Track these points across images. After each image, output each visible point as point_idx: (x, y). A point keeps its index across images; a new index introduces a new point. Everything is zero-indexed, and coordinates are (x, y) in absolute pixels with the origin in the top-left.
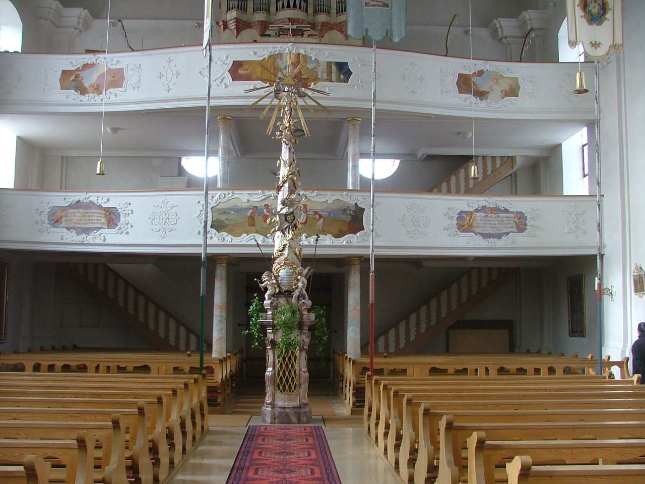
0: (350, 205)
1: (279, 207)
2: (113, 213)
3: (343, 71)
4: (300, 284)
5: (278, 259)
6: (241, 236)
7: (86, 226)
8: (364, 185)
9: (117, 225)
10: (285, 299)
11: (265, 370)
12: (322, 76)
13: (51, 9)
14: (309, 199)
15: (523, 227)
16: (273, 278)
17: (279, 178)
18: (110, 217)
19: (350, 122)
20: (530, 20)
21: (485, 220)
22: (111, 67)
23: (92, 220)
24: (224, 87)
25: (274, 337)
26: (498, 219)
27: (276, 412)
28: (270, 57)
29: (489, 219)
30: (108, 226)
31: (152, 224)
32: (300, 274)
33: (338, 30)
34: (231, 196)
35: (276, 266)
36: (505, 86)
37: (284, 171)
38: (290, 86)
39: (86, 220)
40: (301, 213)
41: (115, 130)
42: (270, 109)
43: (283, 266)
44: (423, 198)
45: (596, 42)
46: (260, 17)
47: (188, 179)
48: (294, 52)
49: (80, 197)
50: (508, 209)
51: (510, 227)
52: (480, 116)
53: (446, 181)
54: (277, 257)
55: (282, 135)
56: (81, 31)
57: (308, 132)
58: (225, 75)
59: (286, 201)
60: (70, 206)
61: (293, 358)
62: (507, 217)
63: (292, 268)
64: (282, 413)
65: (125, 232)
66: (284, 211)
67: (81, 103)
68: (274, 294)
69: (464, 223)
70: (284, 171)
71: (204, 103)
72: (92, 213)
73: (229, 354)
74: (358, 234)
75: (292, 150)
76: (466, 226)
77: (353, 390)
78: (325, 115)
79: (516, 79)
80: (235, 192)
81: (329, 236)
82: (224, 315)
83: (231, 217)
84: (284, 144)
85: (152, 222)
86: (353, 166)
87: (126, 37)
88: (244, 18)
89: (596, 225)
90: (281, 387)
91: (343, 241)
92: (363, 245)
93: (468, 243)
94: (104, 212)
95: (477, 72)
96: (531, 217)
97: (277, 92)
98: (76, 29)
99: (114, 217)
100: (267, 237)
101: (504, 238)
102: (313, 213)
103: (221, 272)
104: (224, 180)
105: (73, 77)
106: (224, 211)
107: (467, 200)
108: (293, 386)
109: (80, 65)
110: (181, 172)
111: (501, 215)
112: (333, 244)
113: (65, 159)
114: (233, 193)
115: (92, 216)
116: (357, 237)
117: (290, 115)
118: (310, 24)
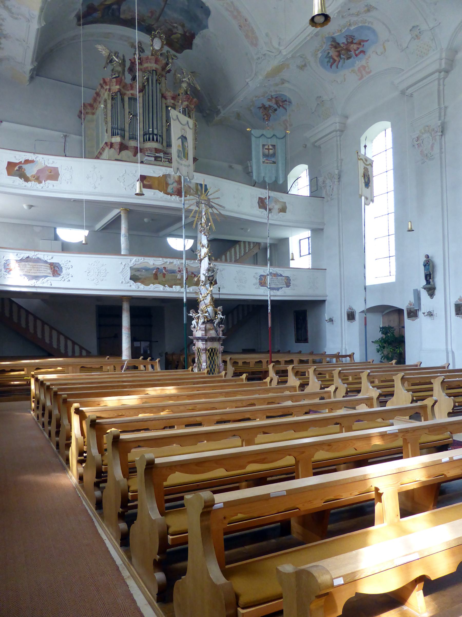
2: (57, 267)
7: (36, 275)
9: (60, 275)
15: (289, 284)
18: (54, 269)
22: (48, 165)
23: (40, 271)
28: (163, 175)
30: (53, 275)
31: (88, 275)
34: (143, 261)
41: (31, 207)
42: (194, 212)
44: (244, 267)
49: (29, 254)
53: (224, 255)
62: (281, 279)
67: (25, 187)
72: (39, 266)
83: (143, 273)
89: (364, 288)
93: (264, 292)
94: (49, 266)
99: (57, 269)
100: (165, 286)
101: (280, 290)
102: (191, 274)
105: (17, 168)
106: (138, 270)
109: (23, 160)
110: (56, 238)
114: (144, 259)
115: (39, 268)
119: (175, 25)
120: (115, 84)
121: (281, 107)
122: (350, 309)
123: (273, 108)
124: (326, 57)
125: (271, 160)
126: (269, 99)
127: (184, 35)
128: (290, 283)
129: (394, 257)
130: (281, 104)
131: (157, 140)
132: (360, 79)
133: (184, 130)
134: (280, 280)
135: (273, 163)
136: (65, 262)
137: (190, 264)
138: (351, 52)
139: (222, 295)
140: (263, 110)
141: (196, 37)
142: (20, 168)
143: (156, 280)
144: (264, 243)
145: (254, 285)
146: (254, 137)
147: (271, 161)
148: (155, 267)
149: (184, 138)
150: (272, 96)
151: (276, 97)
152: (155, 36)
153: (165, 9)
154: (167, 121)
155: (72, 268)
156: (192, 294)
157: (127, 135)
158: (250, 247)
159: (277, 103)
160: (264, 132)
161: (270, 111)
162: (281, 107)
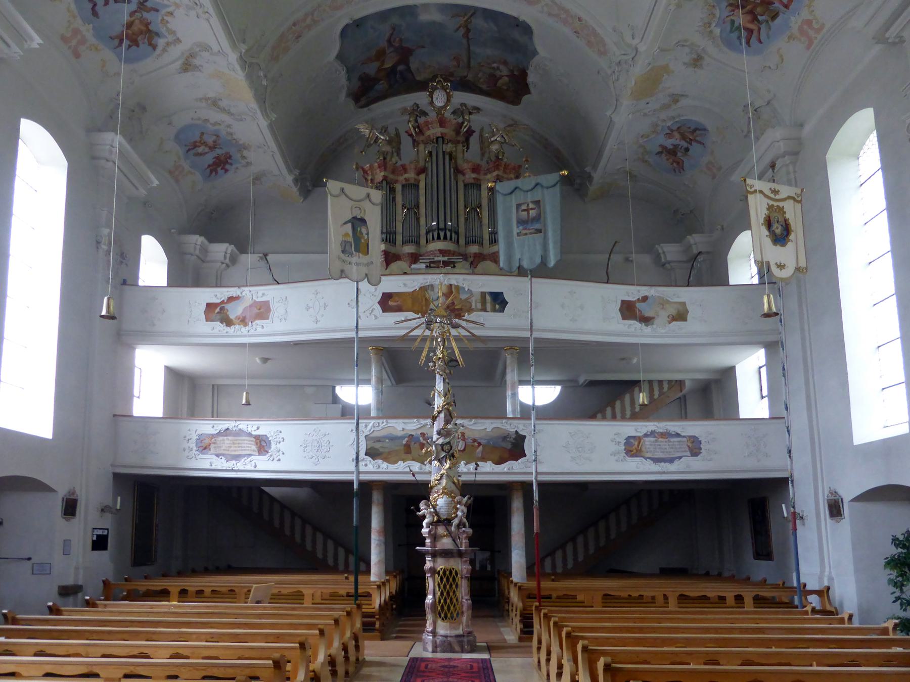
0: (510, 433)
1: (435, 437)
3: (498, 301)
4: (459, 513)
5: (436, 488)
6: (396, 463)
7: (236, 453)
8: (526, 412)
9: (267, 452)
10: (444, 527)
11: (425, 596)
12: (476, 306)
13: (197, 245)
14: (467, 427)
15: (697, 451)
16: (431, 507)
17: (434, 408)
18: (261, 444)
19: (508, 351)
20: (696, 244)
21: (655, 445)
22: (257, 300)
24: (374, 318)
25: (434, 564)
26: (670, 444)
27: (438, 641)
28: (421, 288)
29: (658, 443)
32: (460, 503)
33: (491, 261)
34: (385, 425)
35: (433, 496)
36: (672, 311)
37: (439, 402)
38: (441, 317)
39: (236, 447)
40: (458, 440)
41: (265, 360)
42: (422, 340)
43: (441, 495)
45: (781, 264)
46: (409, 249)
47: (342, 406)
48: (446, 283)
50: (679, 433)
51: (683, 451)
52: (645, 342)
54: (435, 486)
55: (435, 366)
56: (228, 266)
57: (463, 362)
58: (374, 307)
60: (219, 434)
61: (454, 586)
62: (679, 442)
63: (452, 497)
64: (444, 641)
65: (276, 459)
66: (441, 441)
67: (227, 334)
68: (433, 522)
69: (633, 448)
70: (439, 402)
71: (352, 334)
73: (388, 578)
74: (519, 461)
75: (447, 381)
76: (635, 451)
77: (520, 617)
78: (480, 345)
79: (684, 304)
80: (389, 421)
81: (490, 463)
82: (382, 539)
84: (437, 375)
85: (304, 450)
86: (512, 394)
87: (270, 270)
88: (393, 250)
89: (786, 451)
90: (443, 615)
91: (505, 467)
92: (524, 471)
93: (637, 467)
94: (254, 439)
95: (641, 298)
96: (706, 440)
97: (429, 324)
98: (223, 263)
99: (265, 444)
100: (423, 464)
101: (676, 462)
102: (471, 441)
103: (377, 497)
104: (378, 409)
105: (218, 310)
106: (378, 440)
107: (635, 425)
108: (455, 615)
109: (225, 298)
110: (335, 399)
111: (672, 440)
112: (493, 471)
113: (216, 388)
114: (387, 422)
115: (241, 444)
116: (519, 463)
117: (444, 345)
118: (462, 255)
119: (495, 65)
120: (379, 172)
121: (693, 143)
122: (832, 494)
123: (681, 148)
124: (731, 31)
125: (532, 228)
126: (667, 134)
127: (511, 76)
128: (701, 449)
129: (904, 384)
130: (691, 138)
131: (445, 238)
132: (808, 48)
133: (360, 209)
134: (677, 443)
135: (535, 232)
136: (274, 433)
137: (468, 425)
138: (774, 3)
140: (666, 155)
141: (529, 72)
142: (222, 309)
143: (408, 453)
144: (693, 380)
145: (614, 454)
146: (500, 195)
147: (533, 229)
148: (407, 434)
149: (358, 222)
150: (669, 128)
151: (678, 128)
152: (435, 88)
153: (471, 48)
154: (465, 206)
155: (283, 441)
156: (425, 475)
157: (399, 238)
159: (683, 137)
160: (518, 183)
161: (679, 154)
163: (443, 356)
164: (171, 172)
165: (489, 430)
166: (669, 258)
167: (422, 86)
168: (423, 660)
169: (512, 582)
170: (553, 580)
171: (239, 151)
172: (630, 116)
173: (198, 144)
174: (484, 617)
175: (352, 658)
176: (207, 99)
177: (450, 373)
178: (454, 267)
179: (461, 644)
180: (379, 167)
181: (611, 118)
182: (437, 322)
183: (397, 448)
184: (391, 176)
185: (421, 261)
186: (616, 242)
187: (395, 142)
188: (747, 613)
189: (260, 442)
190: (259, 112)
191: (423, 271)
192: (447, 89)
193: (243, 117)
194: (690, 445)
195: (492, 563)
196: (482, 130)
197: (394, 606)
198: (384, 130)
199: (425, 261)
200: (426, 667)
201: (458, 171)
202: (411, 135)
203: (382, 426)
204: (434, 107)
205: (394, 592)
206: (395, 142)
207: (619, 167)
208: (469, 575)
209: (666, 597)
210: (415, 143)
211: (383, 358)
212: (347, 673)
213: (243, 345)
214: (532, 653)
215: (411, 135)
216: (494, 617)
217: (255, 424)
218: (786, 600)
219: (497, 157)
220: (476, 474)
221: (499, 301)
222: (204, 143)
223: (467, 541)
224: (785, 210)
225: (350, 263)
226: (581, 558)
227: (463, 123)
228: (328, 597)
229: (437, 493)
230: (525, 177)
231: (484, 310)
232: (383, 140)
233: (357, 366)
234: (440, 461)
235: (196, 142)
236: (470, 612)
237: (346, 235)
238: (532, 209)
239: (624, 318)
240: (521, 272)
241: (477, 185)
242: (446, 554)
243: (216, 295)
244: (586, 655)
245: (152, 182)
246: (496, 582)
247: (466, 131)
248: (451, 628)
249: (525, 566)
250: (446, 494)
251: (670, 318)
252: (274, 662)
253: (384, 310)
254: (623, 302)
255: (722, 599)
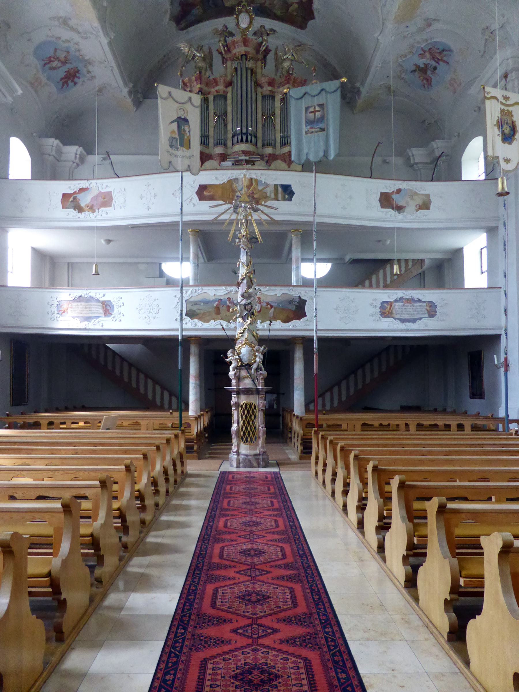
2: (109, 305)
4: (258, 359)
5: (240, 339)
8: (307, 283)
9: (111, 314)
17: (239, 276)
18: (106, 309)
21: (402, 309)
22: (102, 191)
27: (241, 459)
28: (228, 181)
32: (258, 351)
33: (282, 160)
35: (238, 346)
36: (419, 201)
37: (243, 271)
38: (245, 202)
41: (109, 241)
46: (219, 150)
51: (423, 314)
55: (240, 242)
56: (78, 165)
59: (245, 294)
61: (253, 417)
62: (420, 306)
63: (251, 347)
65: (118, 320)
66: (244, 302)
70: (243, 271)
71: (177, 219)
73: (202, 413)
75: (249, 254)
76: (387, 313)
79: (428, 196)
81: (279, 321)
82: (198, 382)
83: (200, 307)
84: (242, 250)
88: (207, 151)
90: (244, 439)
97: (236, 208)
98: (74, 163)
99: (109, 308)
100: (229, 322)
101: (418, 322)
103: (194, 349)
104: (195, 279)
105: (71, 199)
106: (196, 303)
108: (254, 439)
110: (162, 274)
111: (415, 304)
114: (202, 289)
115: (92, 308)
121: (441, 63)
126: (421, 54)
128: (436, 312)
129: (486, 249)
130: (439, 58)
131: (247, 141)
133: (184, 110)
139: (274, 332)
142: (75, 198)
144: (430, 259)
149: (182, 121)
151: (430, 49)
152: (240, 12)
154: (262, 114)
157: (211, 141)
158: (408, 265)
159: (433, 58)
161: (429, 72)
162: (441, 63)
163: (247, 233)
164: (31, 84)
165: (279, 295)
166: (417, 160)
167: (230, 11)
168: (230, 473)
169: (294, 414)
170: (324, 414)
171: (85, 66)
172: (393, 38)
173: (52, 59)
174: (272, 443)
175: (179, 472)
176: (59, 18)
177: (251, 247)
178: (254, 164)
179: (258, 460)
180: (196, 80)
181: (378, 39)
182: (241, 207)
183: (211, 310)
184: (205, 88)
185: (228, 160)
186: (379, 143)
187: (208, 59)
188: (466, 435)
189: (106, 306)
190: (100, 30)
191: (230, 168)
192: (250, 12)
193: (88, 35)
194: (428, 308)
195: (278, 404)
196: (276, 49)
197: (206, 435)
198: (200, 49)
199: (232, 160)
200: (233, 477)
201: (258, 84)
202: (221, 53)
203: (198, 292)
204: (240, 29)
205: (206, 425)
206: (208, 59)
207: (382, 83)
208: (264, 408)
209: (407, 425)
210: (224, 60)
211: (199, 239)
212: (176, 481)
213: (92, 228)
214: (310, 467)
215: (221, 53)
216: (279, 443)
217: (101, 292)
218: (494, 428)
219: (288, 72)
220: (270, 330)
221: (288, 192)
222: (58, 58)
223: (263, 381)
224: (513, 114)
225: (176, 156)
226: (344, 399)
227: (262, 43)
228: (157, 427)
229: (241, 343)
230: (313, 84)
231: (277, 199)
232: (199, 57)
233: (181, 240)
234: (244, 318)
235: (50, 57)
236: (265, 436)
237: (173, 132)
238: (318, 111)
239: (382, 206)
240: (306, 167)
241: (272, 97)
242: (248, 391)
243: (70, 187)
244: (356, 462)
245: (17, 91)
246: (281, 418)
247: (264, 50)
248: (251, 449)
249: (304, 403)
250: (248, 344)
251: (418, 207)
252: (126, 467)
253: (200, 199)
254: (382, 194)
255: (447, 427)
